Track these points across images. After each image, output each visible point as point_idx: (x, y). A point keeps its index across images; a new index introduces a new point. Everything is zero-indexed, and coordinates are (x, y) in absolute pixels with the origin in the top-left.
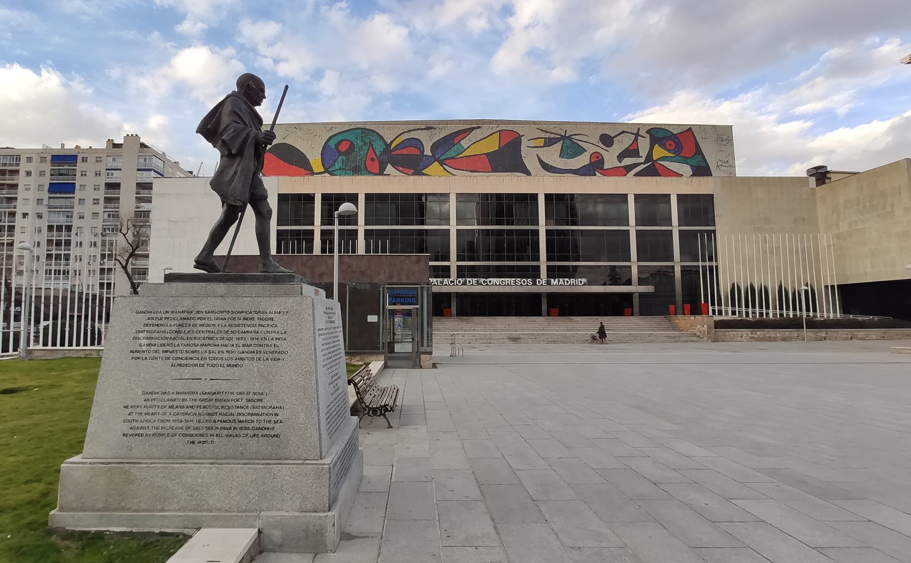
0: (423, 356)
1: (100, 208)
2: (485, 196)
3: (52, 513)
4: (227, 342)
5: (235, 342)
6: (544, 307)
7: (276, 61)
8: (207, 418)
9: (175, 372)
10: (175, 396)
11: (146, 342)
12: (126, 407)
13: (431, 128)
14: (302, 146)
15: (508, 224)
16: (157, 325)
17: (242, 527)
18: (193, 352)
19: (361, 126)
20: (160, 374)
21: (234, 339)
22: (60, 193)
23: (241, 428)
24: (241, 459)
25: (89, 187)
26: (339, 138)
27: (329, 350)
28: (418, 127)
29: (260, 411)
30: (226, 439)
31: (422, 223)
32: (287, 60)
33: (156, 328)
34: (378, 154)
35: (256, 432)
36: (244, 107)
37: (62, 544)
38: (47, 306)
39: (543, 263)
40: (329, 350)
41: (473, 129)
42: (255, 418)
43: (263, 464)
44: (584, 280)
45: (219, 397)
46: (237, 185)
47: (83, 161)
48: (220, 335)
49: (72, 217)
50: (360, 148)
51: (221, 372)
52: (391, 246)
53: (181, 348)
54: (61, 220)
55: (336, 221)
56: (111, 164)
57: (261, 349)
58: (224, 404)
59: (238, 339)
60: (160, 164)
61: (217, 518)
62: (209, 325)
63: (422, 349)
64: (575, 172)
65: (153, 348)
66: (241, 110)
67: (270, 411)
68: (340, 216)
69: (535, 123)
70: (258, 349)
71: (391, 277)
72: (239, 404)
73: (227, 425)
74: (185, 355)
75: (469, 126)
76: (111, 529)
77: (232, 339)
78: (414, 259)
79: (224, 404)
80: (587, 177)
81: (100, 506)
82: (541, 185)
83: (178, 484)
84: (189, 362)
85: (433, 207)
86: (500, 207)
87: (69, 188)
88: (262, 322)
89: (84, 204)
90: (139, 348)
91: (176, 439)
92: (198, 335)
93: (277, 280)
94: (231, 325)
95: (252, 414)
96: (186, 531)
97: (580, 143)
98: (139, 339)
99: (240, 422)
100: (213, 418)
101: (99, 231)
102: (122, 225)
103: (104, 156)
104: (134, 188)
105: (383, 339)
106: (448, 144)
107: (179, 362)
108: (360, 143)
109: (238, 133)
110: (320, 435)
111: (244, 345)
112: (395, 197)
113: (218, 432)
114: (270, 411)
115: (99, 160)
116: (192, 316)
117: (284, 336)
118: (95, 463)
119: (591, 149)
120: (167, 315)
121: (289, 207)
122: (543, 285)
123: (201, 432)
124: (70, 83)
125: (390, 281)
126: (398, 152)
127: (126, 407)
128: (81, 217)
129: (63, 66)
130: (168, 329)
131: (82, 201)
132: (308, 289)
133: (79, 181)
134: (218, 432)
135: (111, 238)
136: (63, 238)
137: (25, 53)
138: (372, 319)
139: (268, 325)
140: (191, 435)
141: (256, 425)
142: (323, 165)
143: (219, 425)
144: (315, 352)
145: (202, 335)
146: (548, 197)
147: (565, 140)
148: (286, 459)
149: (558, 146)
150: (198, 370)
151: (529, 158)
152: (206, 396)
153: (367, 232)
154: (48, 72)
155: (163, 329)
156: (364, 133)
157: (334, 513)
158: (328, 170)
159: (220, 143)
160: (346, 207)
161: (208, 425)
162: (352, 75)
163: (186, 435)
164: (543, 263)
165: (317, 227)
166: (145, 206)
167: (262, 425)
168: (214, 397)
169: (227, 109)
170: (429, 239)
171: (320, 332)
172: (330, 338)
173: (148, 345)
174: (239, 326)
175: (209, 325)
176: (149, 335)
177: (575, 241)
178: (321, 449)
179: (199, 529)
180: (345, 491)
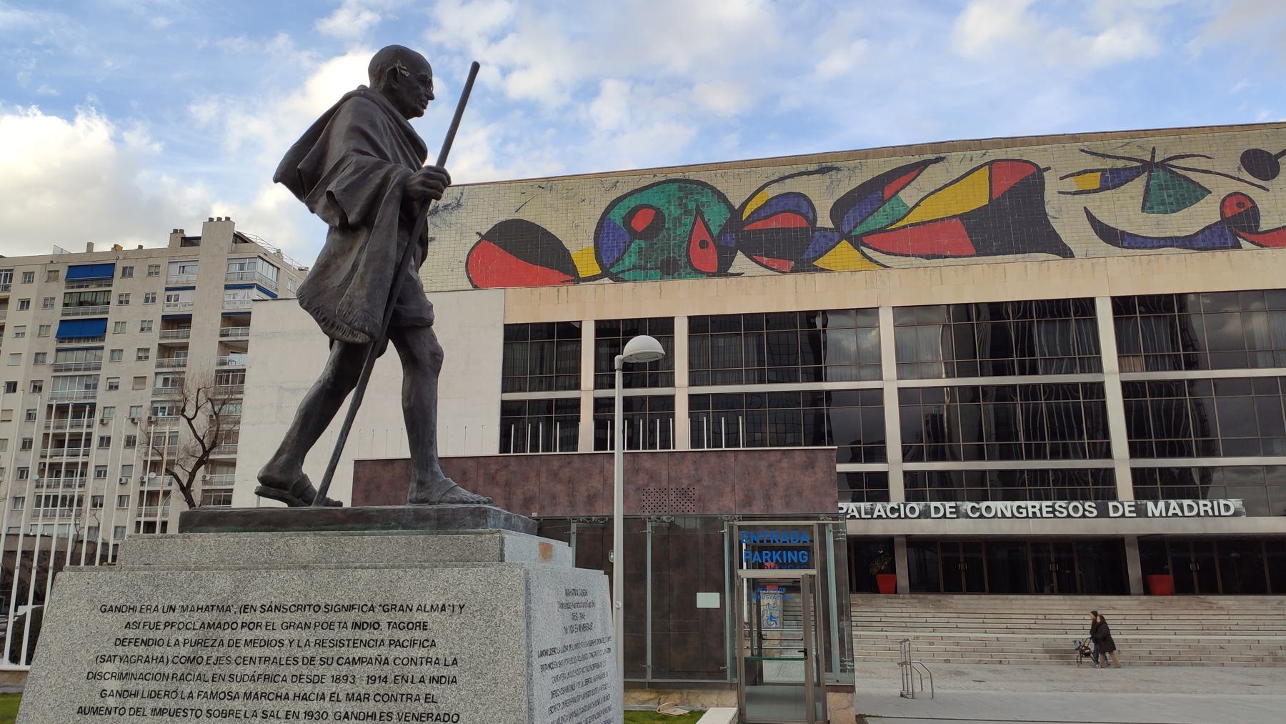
0: (832, 698)
1: (149, 368)
2: (963, 310)
4: (308, 688)
5: (328, 687)
6: (1134, 571)
7: (505, 71)
11: (113, 685)
13: (830, 169)
15: (1022, 373)
16: (146, 643)
19: (679, 176)
21: (328, 680)
22: (79, 339)
25: (132, 323)
27: (573, 707)
28: (802, 168)
31: (818, 377)
32: (525, 67)
33: (141, 651)
34: (715, 230)
36: (380, 118)
38: (26, 568)
39: (1122, 463)
40: (573, 707)
41: (926, 164)
44: (1235, 504)
46: (357, 293)
47: (124, 275)
48: (293, 669)
49: (95, 387)
50: (677, 221)
52: (748, 432)
53: (198, 703)
54: (74, 393)
55: (619, 377)
56: (176, 278)
59: (336, 679)
60: (270, 273)
62: (267, 643)
63: (829, 678)
64: (1187, 243)
65: (131, 702)
66: (373, 125)
68: (626, 367)
69: (1074, 138)
71: (748, 501)
75: (917, 159)
77: (320, 679)
78: (800, 458)
80: (1219, 254)
82: (1102, 278)
85: (840, 339)
86: (996, 334)
87: (96, 329)
88: (401, 635)
89: (120, 359)
90: (99, 702)
93: (444, 523)
94: (321, 643)
97: (1191, 175)
98: (102, 676)
101: (145, 413)
102: (186, 400)
103: (163, 263)
105: (737, 649)
106: (872, 201)
108: (675, 211)
109: (363, 175)
111: (349, 698)
112: (753, 321)
115: (154, 271)
116: (229, 618)
117: (451, 671)
119: (1221, 188)
120: (171, 617)
121: (528, 352)
122: (1126, 517)
124: (125, 134)
125: (746, 512)
126: (759, 225)
128: (113, 387)
129: (115, 107)
130: (170, 652)
131: (116, 353)
132: (522, 545)
133: (114, 314)
135: (159, 429)
136: (68, 431)
137: (53, 92)
138: (708, 600)
139: (413, 643)
145: (249, 669)
146: (1122, 306)
147: (1153, 169)
149: (1136, 187)
151: (1065, 215)
153: (694, 401)
154: (88, 116)
155: (157, 651)
156: (685, 186)
158: (610, 270)
159: (323, 200)
160: (641, 345)
162: (656, 85)
164: (1122, 463)
165: (587, 394)
166: (236, 361)
169: (341, 125)
170: (835, 411)
171: (547, 660)
172: (578, 672)
173: (121, 694)
174: (340, 643)
175: (267, 643)
176: (125, 667)
177: (1198, 405)
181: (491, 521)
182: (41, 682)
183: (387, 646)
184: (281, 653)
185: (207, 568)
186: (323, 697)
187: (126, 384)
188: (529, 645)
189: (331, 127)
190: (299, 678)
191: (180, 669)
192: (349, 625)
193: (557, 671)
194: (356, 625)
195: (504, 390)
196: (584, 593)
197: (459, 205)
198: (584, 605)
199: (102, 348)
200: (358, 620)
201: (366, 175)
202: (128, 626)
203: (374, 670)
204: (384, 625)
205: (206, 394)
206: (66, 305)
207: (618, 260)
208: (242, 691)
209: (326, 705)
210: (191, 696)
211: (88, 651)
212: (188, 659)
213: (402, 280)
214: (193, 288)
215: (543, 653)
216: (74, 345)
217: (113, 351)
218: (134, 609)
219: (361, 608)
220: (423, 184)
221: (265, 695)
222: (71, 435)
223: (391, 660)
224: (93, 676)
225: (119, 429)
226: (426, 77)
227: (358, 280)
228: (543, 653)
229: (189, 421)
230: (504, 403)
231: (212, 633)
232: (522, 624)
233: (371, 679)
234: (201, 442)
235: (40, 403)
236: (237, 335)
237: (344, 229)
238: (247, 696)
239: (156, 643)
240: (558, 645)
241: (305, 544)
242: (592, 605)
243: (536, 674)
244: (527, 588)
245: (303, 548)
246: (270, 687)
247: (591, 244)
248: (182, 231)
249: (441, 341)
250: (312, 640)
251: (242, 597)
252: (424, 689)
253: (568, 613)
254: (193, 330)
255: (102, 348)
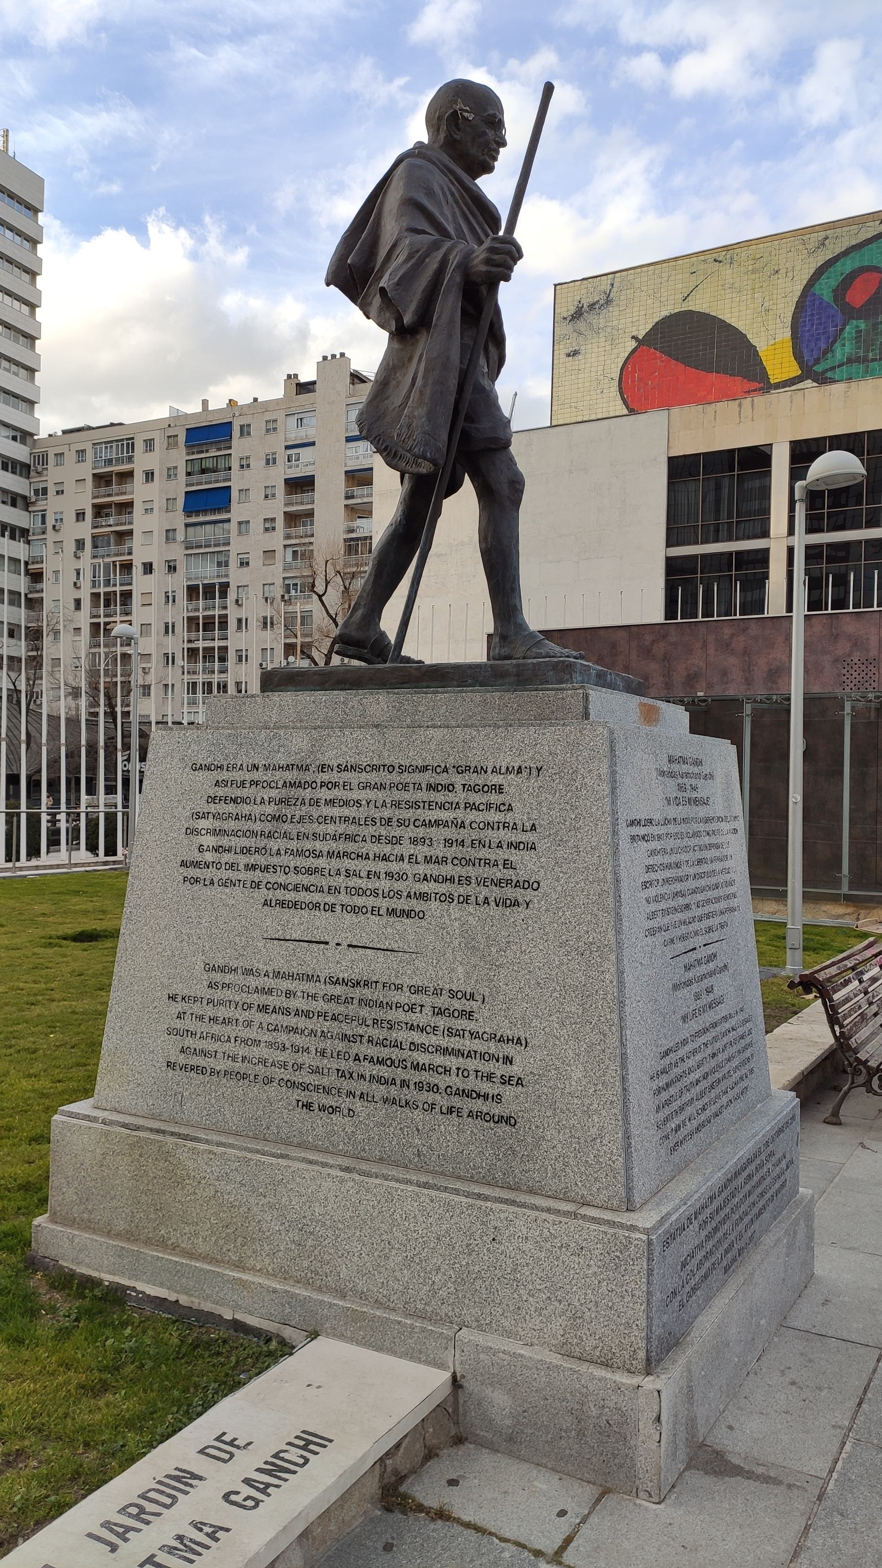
1: (277, 540)
3: (37, 1221)
4: (387, 849)
5: (406, 849)
8: (341, 1046)
9: (274, 921)
10: (270, 982)
11: (209, 841)
12: (172, 998)
14: (737, 313)
16: (234, 801)
17: (412, 1358)
18: (310, 871)
20: (239, 924)
21: (406, 842)
22: (205, 512)
23: (419, 1086)
24: (418, 1169)
25: (255, 494)
26: (848, 266)
29: (467, 1044)
30: (382, 1111)
33: (231, 808)
35: (456, 1101)
37: (45, 1296)
42: (453, 1062)
43: (468, 1195)
45: (367, 993)
51: (372, 928)
53: (284, 860)
54: (207, 573)
56: (296, 435)
57: (471, 871)
58: (379, 1014)
59: (414, 841)
61: (357, 1317)
62: (346, 803)
65: (226, 857)
66: (430, 193)
67: (493, 1047)
70: (463, 871)
72: (415, 1018)
73: (385, 1072)
74: (293, 879)
76: (140, 1286)
77: (398, 841)
79: (379, 1014)
81: (121, 1225)
83: (271, 1206)
84: (304, 896)
87: (102, 480)
90: (198, 857)
91: (272, 1090)
92: (321, 829)
94: (397, 805)
95: (446, 1051)
96: (288, 1333)
99: (416, 1067)
100: (355, 1049)
102: (314, 575)
104: (340, 483)
107: (280, 894)
110: (627, 1136)
111: (428, 860)
113: (363, 1086)
114: (493, 1047)
115: (271, 428)
116: (308, 777)
117: (530, 837)
118: (111, 1123)
120: (256, 775)
121: (697, 489)
123: (325, 1081)
127: (172, 998)
128: (244, 564)
130: (257, 810)
133: (237, 481)
134: (363, 1086)
135: (290, 609)
139: (489, 806)
140: (305, 1087)
141: (456, 1081)
142: (798, 355)
143: (368, 1069)
144: (617, 889)
145: (331, 829)
148: (531, 1192)
150: (322, 918)
152: (338, 990)
155: (246, 809)
157: (666, 1383)
158: (813, 368)
159: (377, 301)
161: (343, 1065)
163: (294, 1085)
167: (472, 1083)
168: (357, 993)
173: (216, 849)
174: (415, 805)
175: (346, 803)
176: (217, 824)
178: (629, 1178)
179: (314, 1335)
180: (721, 1314)
181: (577, 677)
182: (147, 836)
183: (462, 810)
184: (361, 813)
185: (285, 727)
186: (402, 859)
187: (256, 560)
188: (614, 813)
189: (382, 203)
190: (378, 839)
191: (268, 827)
192: (424, 786)
193: (654, 845)
194: (431, 787)
195: (669, 545)
196: (698, 763)
197: (608, 301)
198: (698, 776)
199: (229, 520)
200: (432, 781)
201: (421, 262)
202: (217, 784)
203: (450, 833)
204: (458, 787)
205: (334, 566)
206: (189, 474)
207: (825, 353)
208: (325, 850)
209: (405, 866)
210: (278, 853)
211: (184, 808)
212: (274, 817)
213: (468, 395)
214: (313, 444)
215: (632, 823)
216: (201, 519)
217: (240, 523)
218: (221, 767)
219: (434, 769)
220: (487, 262)
221: (346, 854)
222: (204, 617)
223: (467, 823)
224: (192, 832)
225: (254, 608)
226: (494, 116)
227: (417, 396)
228: (632, 823)
229: (320, 597)
230: (669, 560)
231: (293, 792)
232: (606, 788)
233: (449, 842)
234: (334, 621)
235: (178, 583)
236: (363, 496)
237: (403, 334)
238: (330, 854)
239: (244, 801)
240: (657, 816)
241: (378, 703)
242: (710, 776)
243: (624, 844)
244: (612, 749)
245: (376, 707)
246: (351, 847)
247: (786, 334)
248: (296, 376)
249: (522, 465)
250: (388, 801)
251: (319, 756)
252: (502, 854)
253: (671, 783)
254: (317, 495)
255: (229, 520)
